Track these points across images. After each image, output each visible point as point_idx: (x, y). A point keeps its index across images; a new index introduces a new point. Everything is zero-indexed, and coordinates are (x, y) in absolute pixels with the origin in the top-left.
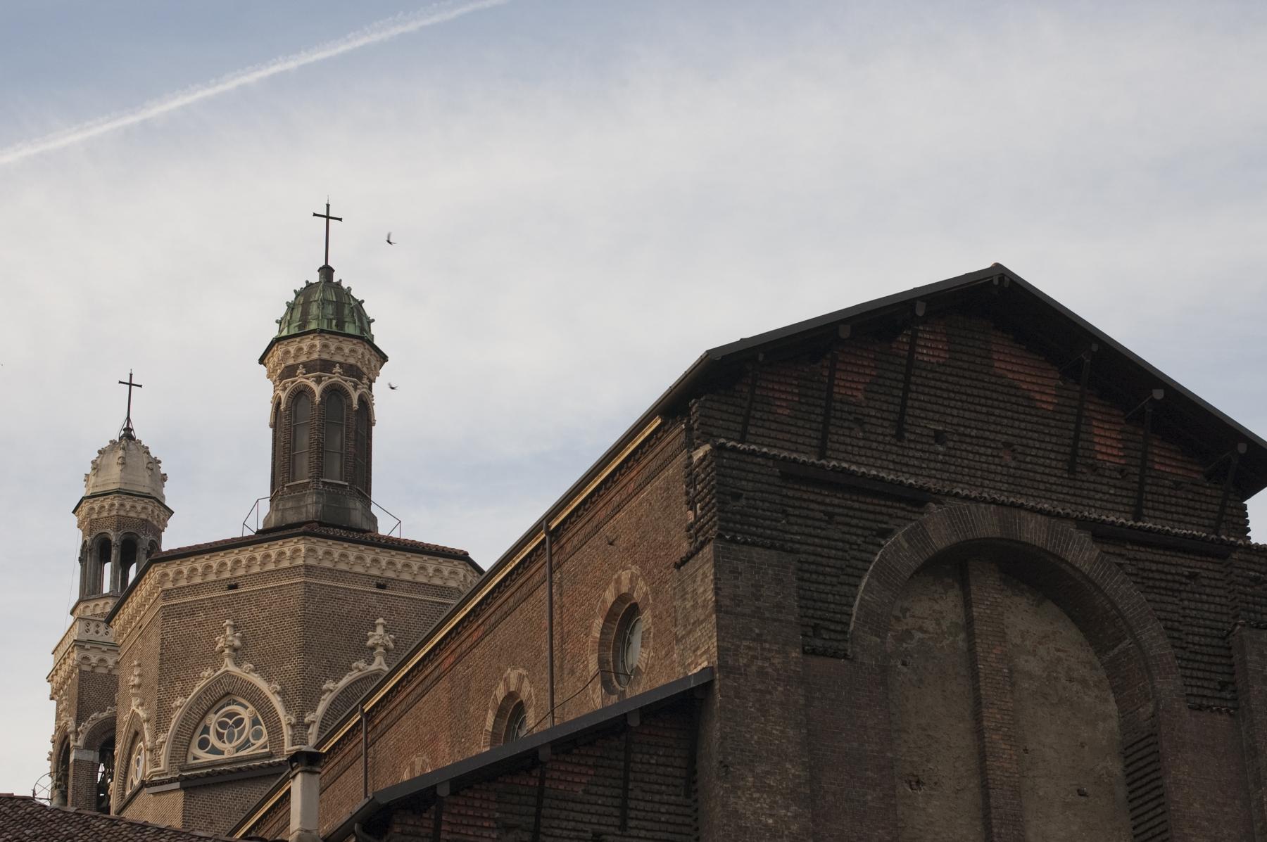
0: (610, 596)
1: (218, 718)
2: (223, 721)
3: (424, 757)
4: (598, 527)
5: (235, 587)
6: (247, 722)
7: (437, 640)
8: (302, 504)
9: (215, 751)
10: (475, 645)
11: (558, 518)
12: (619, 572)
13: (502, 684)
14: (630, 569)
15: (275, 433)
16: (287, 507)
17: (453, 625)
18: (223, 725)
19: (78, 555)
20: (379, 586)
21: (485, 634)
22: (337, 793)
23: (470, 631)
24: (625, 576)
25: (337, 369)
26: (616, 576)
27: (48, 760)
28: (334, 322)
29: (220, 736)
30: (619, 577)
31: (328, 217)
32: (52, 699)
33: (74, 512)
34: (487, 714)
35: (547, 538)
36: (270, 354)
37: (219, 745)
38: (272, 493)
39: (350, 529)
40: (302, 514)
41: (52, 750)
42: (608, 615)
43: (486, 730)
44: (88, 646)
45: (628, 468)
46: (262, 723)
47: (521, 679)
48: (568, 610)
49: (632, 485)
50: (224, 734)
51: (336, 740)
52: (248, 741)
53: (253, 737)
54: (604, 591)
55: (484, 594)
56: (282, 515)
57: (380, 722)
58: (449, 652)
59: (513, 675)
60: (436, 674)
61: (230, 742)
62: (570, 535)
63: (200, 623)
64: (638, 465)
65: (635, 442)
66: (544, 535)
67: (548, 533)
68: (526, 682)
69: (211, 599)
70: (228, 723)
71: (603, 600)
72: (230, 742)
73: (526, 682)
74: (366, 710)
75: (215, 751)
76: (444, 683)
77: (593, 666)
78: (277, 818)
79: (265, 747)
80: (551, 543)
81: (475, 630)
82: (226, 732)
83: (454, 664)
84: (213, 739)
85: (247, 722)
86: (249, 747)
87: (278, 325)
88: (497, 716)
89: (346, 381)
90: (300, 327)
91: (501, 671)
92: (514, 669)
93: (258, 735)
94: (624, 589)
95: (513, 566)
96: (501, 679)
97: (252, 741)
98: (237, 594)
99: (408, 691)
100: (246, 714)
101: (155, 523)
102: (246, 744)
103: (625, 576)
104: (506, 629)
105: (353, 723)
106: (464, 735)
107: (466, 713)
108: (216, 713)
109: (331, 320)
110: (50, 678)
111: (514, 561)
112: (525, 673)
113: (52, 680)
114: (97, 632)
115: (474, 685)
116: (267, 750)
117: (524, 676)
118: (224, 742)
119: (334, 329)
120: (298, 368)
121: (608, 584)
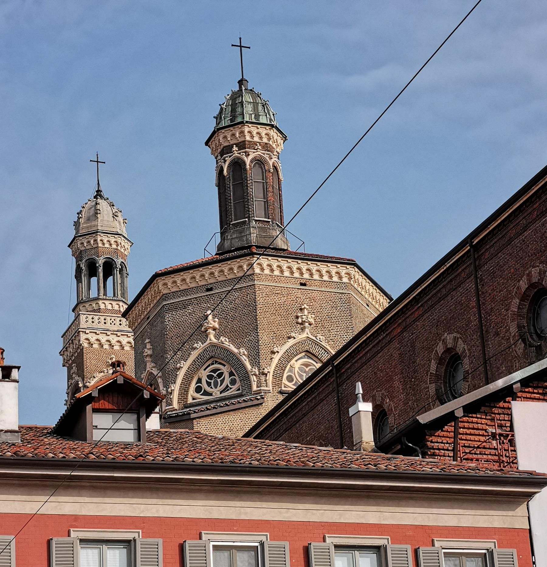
0: (523, 285)
1: (207, 372)
2: (223, 374)
3: (383, 391)
4: (511, 240)
5: (211, 289)
6: (226, 375)
7: (389, 317)
8: (243, 234)
9: (206, 393)
10: (417, 320)
11: (479, 237)
12: (530, 269)
13: (441, 344)
14: (538, 266)
15: (219, 189)
16: (233, 237)
17: (400, 308)
18: (210, 377)
19: (74, 273)
20: (302, 284)
21: (426, 312)
22: (315, 416)
23: (412, 311)
24: (535, 272)
25: (235, 148)
26: (527, 272)
27: (65, 405)
28: (253, 116)
29: (209, 384)
30: (530, 272)
31: (241, 46)
32: (64, 366)
33: (69, 246)
34: (431, 362)
35: (472, 249)
36: (213, 139)
37: (208, 389)
38: (221, 228)
39: (275, 249)
40: (244, 242)
41: (359, 403)
42: (523, 297)
43: (431, 373)
44: (87, 331)
45: (532, 202)
46: (236, 375)
47: (455, 339)
48: (490, 295)
49: (536, 213)
50: (211, 382)
51: (314, 383)
52: (227, 386)
53: (230, 384)
54: (519, 281)
55: (423, 287)
56: (231, 242)
57: (345, 371)
58: (396, 325)
59: (449, 338)
60: (388, 338)
61: (216, 388)
62: (488, 247)
63: (190, 313)
64: (540, 200)
65: (538, 185)
66: (469, 248)
67: (471, 246)
68: (460, 341)
69: (196, 298)
70: (213, 376)
71: (518, 287)
72: (216, 388)
73: (460, 341)
74: (335, 364)
75: (206, 393)
76: (396, 344)
77: (513, 329)
78: (270, 434)
79: (239, 390)
80: (474, 252)
81: (416, 310)
82: (212, 381)
83: (402, 332)
84: (204, 386)
85: (226, 375)
86: (228, 390)
87: (215, 120)
88: (438, 364)
89: (264, 154)
90: (232, 120)
91: (439, 336)
92: (449, 333)
93: (233, 382)
94: (535, 280)
95: (445, 268)
96: (440, 340)
97: (230, 386)
98: (212, 294)
99: (366, 350)
100: (225, 370)
101: (122, 250)
102: (227, 389)
103: (535, 272)
104: (441, 309)
105: (326, 372)
106: (414, 377)
107: (414, 362)
108: (205, 370)
109: (251, 114)
110: (61, 353)
111: (446, 266)
112: (459, 336)
113: (63, 354)
114: (120, 324)
115: (418, 345)
116: (240, 391)
117: (458, 338)
118: (211, 388)
119: (254, 120)
120: (233, 147)
121: (522, 277)
